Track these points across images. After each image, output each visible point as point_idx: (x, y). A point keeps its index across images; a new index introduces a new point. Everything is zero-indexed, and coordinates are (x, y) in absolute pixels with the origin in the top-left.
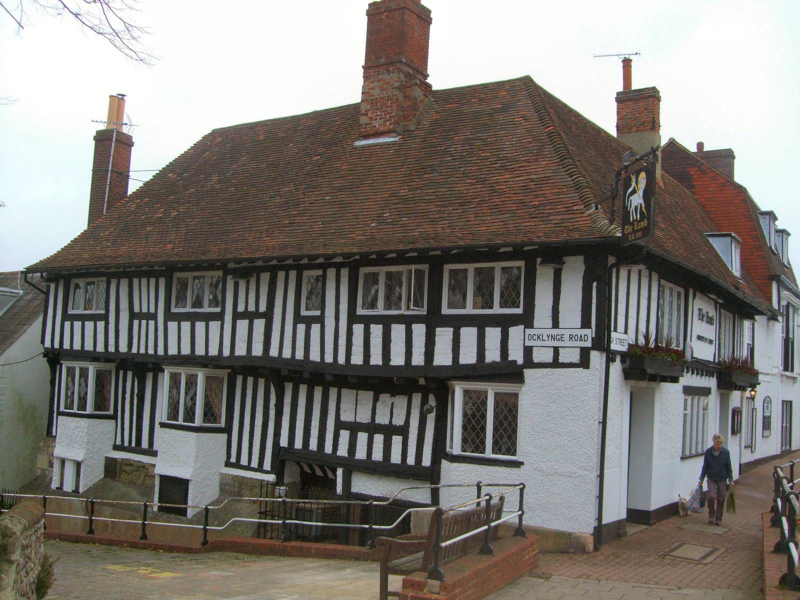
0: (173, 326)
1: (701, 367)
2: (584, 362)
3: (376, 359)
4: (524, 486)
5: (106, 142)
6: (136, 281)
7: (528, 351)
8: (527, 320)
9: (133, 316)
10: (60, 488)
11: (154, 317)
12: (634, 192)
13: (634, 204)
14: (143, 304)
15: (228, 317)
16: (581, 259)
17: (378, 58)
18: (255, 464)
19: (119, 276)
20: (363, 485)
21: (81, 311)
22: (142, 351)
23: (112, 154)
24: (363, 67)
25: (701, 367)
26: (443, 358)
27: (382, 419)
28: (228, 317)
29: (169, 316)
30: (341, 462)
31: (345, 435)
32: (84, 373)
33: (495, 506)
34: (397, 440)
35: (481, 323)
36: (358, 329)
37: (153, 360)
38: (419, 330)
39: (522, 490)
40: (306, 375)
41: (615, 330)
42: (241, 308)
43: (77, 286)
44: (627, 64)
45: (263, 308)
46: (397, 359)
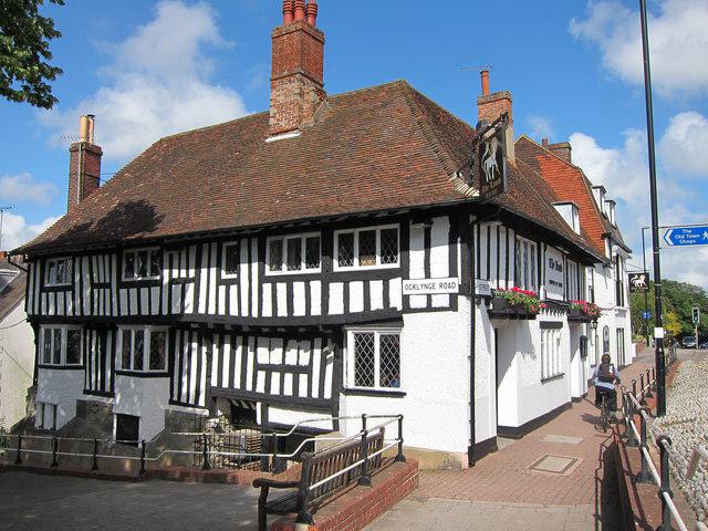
0: (123, 292)
1: (552, 306)
2: (453, 306)
3: (316, 310)
4: (402, 417)
6: (94, 258)
7: (406, 299)
8: (403, 273)
10: (42, 426)
11: (108, 286)
12: (488, 156)
13: (489, 166)
16: (447, 218)
19: (81, 254)
20: (277, 416)
21: (54, 284)
22: (101, 314)
25: (552, 306)
26: (336, 308)
29: (121, 285)
30: (260, 397)
31: (262, 375)
32: (58, 332)
33: (374, 438)
34: (303, 378)
35: (366, 277)
36: (267, 287)
37: (235, 322)
38: (316, 286)
39: (400, 421)
41: (479, 277)
43: (52, 265)
46: (299, 311)
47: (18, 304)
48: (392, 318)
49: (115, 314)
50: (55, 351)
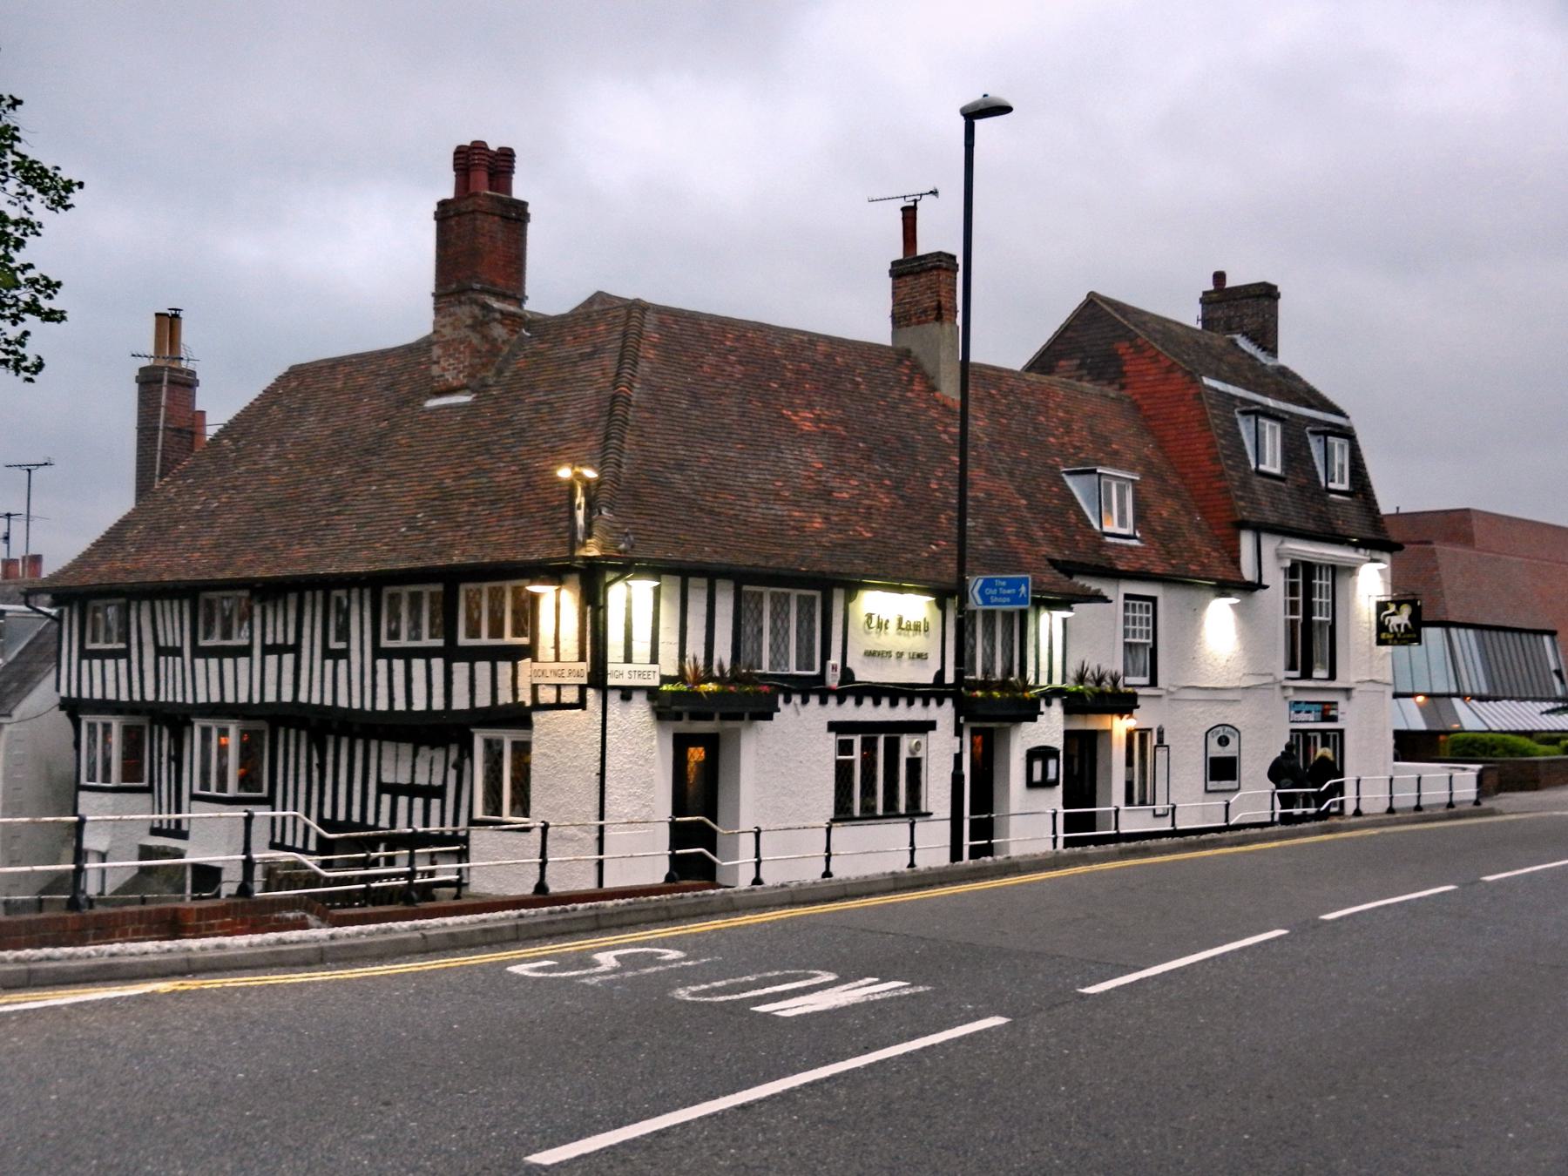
0: (200, 663)
2: (581, 704)
5: (154, 385)
6: (158, 604)
9: (160, 651)
14: (169, 638)
15: (257, 652)
17: (449, 283)
18: (299, 845)
23: (163, 404)
24: (433, 294)
27: (422, 779)
28: (257, 652)
29: (198, 652)
40: (335, 725)
42: (269, 641)
43: (96, 610)
44: (909, 215)
45: (291, 640)
47: (49, 672)
48: (518, 717)
49: (190, 700)
50: (874, 793)
